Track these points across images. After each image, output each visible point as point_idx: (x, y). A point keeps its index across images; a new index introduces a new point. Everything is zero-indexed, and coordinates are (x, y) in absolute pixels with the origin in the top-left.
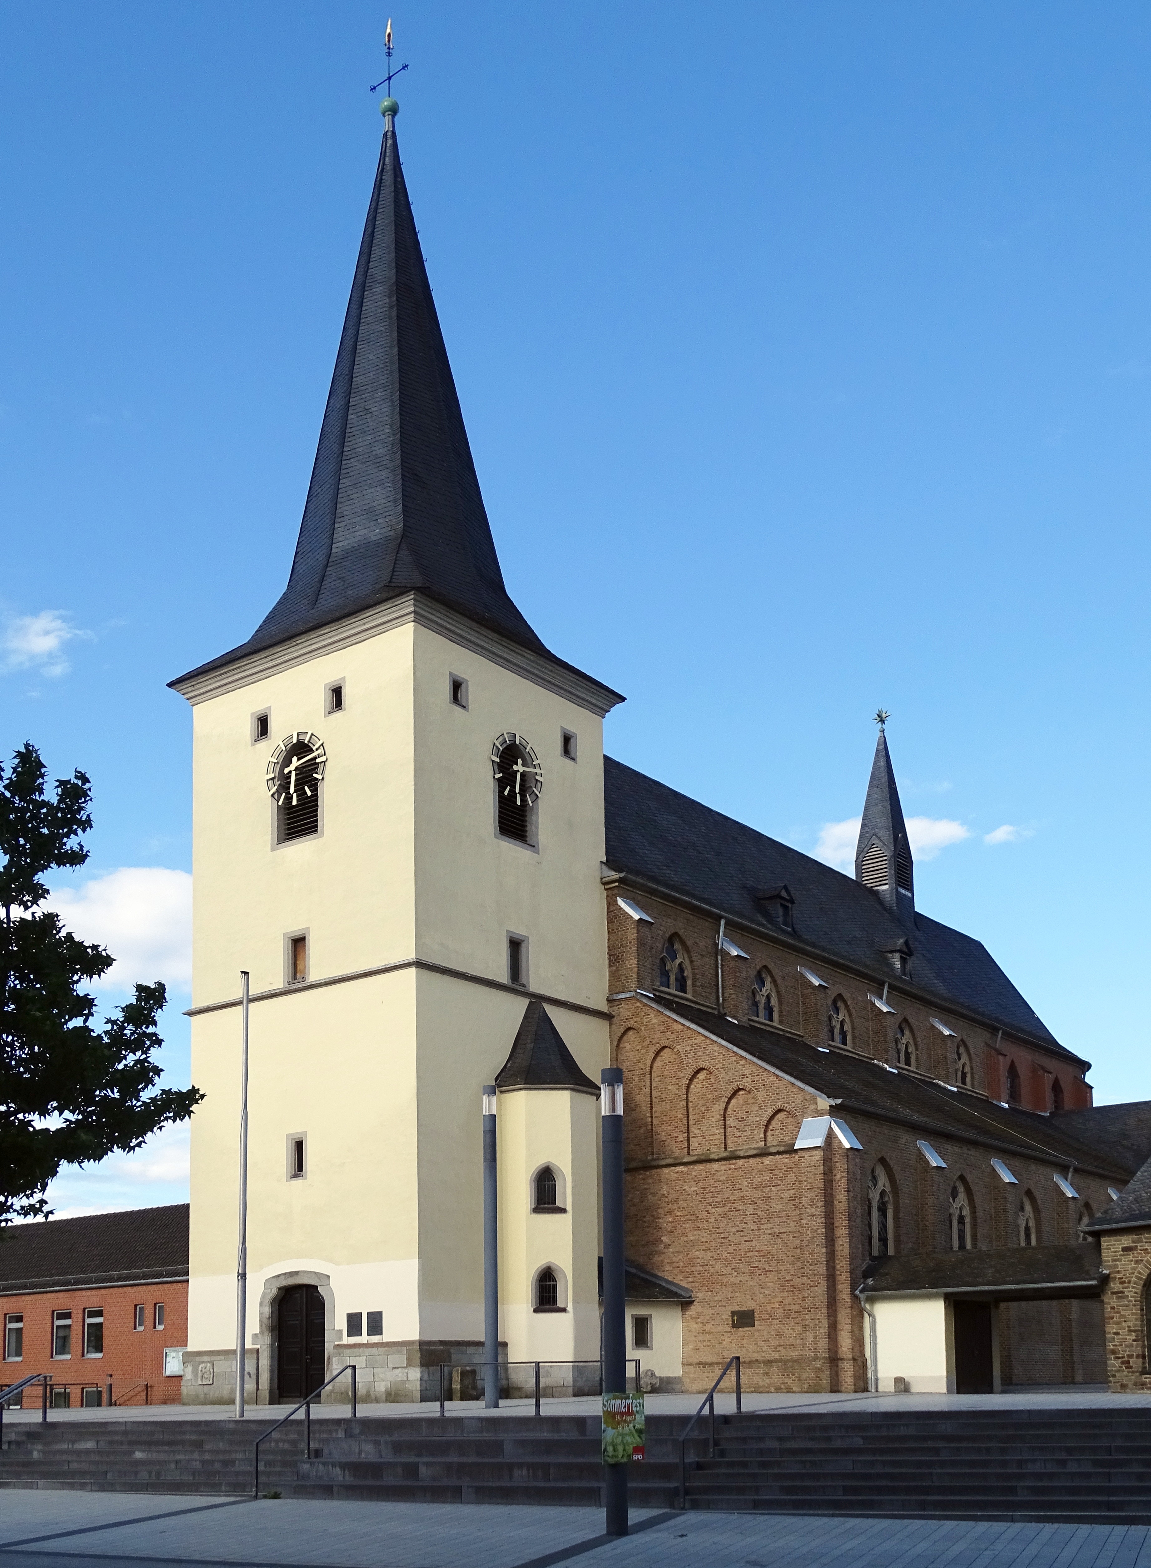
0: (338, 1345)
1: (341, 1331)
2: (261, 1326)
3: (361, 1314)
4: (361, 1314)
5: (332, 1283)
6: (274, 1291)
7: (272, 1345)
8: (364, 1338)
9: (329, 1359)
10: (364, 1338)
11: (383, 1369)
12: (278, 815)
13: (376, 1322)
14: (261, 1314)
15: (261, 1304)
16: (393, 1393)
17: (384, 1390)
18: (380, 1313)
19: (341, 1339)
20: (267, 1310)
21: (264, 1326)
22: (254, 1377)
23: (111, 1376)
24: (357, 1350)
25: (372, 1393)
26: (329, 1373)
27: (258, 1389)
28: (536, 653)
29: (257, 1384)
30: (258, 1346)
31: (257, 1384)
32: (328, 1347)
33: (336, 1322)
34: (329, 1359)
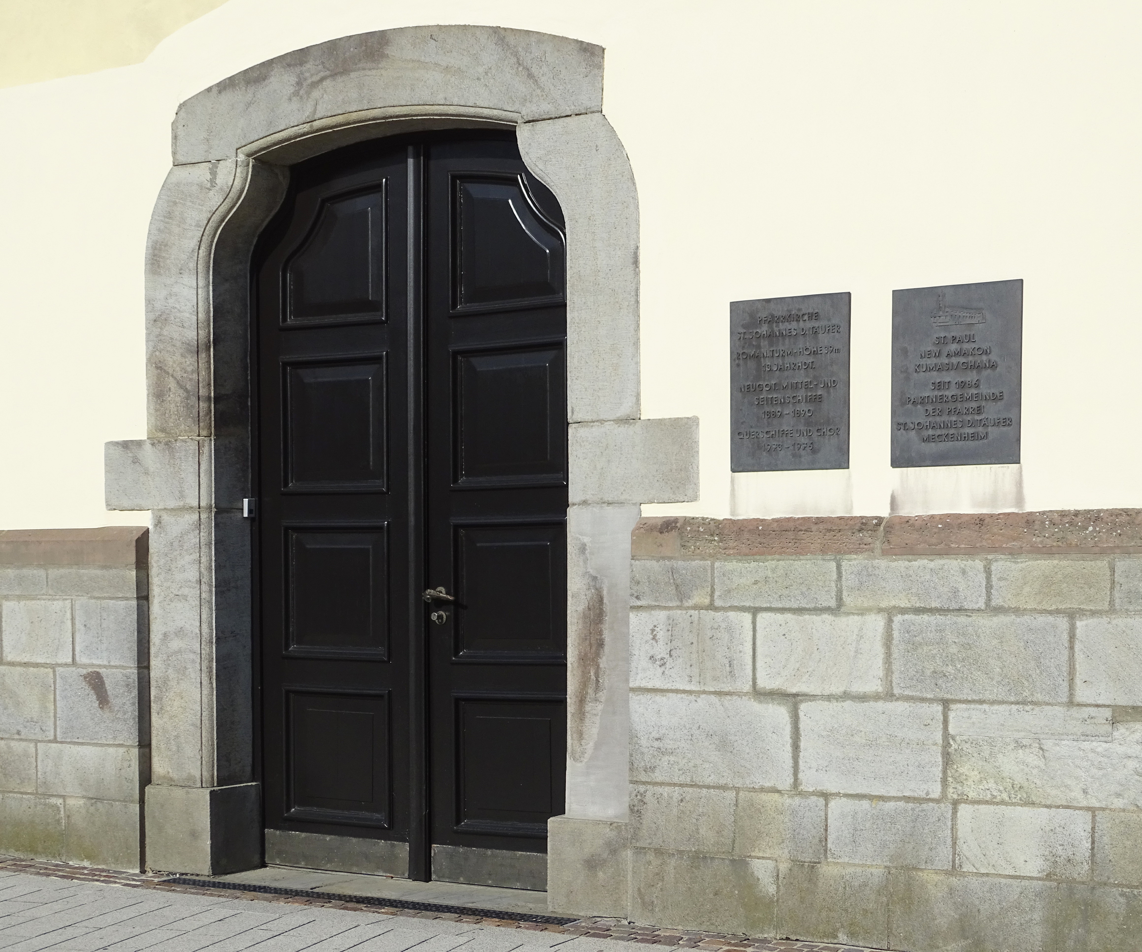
0: (668, 525)
1: (680, 433)
2: (158, 394)
3: (841, 302)
4: (841, 302)
5: (623, 97)
6: (233, 176)
7: (223, 510)
8: (868, 479)
9: (596, 614)
10: (868, 479)
11: (1031, 719)
12: (159, 198)
13: (964, 367)
14: (158, 320)
15: (156, 260)
16: (1114, 901)
17: (1033, 866)
18: (1003, 300)
19: (682, 479)
20: (192, 297)
21: (175, 397)
22: (126, 701)
23: (780, 625)
24: (813, 571)
25: (932, 880)
26: (595, 709)
27: (146, 777)
28: (149, 634)
29: (145, 743)
30: (143, 520)
31: (145, 743)
32: (597, 537)
33: (649, 368)
34: (596, 614)
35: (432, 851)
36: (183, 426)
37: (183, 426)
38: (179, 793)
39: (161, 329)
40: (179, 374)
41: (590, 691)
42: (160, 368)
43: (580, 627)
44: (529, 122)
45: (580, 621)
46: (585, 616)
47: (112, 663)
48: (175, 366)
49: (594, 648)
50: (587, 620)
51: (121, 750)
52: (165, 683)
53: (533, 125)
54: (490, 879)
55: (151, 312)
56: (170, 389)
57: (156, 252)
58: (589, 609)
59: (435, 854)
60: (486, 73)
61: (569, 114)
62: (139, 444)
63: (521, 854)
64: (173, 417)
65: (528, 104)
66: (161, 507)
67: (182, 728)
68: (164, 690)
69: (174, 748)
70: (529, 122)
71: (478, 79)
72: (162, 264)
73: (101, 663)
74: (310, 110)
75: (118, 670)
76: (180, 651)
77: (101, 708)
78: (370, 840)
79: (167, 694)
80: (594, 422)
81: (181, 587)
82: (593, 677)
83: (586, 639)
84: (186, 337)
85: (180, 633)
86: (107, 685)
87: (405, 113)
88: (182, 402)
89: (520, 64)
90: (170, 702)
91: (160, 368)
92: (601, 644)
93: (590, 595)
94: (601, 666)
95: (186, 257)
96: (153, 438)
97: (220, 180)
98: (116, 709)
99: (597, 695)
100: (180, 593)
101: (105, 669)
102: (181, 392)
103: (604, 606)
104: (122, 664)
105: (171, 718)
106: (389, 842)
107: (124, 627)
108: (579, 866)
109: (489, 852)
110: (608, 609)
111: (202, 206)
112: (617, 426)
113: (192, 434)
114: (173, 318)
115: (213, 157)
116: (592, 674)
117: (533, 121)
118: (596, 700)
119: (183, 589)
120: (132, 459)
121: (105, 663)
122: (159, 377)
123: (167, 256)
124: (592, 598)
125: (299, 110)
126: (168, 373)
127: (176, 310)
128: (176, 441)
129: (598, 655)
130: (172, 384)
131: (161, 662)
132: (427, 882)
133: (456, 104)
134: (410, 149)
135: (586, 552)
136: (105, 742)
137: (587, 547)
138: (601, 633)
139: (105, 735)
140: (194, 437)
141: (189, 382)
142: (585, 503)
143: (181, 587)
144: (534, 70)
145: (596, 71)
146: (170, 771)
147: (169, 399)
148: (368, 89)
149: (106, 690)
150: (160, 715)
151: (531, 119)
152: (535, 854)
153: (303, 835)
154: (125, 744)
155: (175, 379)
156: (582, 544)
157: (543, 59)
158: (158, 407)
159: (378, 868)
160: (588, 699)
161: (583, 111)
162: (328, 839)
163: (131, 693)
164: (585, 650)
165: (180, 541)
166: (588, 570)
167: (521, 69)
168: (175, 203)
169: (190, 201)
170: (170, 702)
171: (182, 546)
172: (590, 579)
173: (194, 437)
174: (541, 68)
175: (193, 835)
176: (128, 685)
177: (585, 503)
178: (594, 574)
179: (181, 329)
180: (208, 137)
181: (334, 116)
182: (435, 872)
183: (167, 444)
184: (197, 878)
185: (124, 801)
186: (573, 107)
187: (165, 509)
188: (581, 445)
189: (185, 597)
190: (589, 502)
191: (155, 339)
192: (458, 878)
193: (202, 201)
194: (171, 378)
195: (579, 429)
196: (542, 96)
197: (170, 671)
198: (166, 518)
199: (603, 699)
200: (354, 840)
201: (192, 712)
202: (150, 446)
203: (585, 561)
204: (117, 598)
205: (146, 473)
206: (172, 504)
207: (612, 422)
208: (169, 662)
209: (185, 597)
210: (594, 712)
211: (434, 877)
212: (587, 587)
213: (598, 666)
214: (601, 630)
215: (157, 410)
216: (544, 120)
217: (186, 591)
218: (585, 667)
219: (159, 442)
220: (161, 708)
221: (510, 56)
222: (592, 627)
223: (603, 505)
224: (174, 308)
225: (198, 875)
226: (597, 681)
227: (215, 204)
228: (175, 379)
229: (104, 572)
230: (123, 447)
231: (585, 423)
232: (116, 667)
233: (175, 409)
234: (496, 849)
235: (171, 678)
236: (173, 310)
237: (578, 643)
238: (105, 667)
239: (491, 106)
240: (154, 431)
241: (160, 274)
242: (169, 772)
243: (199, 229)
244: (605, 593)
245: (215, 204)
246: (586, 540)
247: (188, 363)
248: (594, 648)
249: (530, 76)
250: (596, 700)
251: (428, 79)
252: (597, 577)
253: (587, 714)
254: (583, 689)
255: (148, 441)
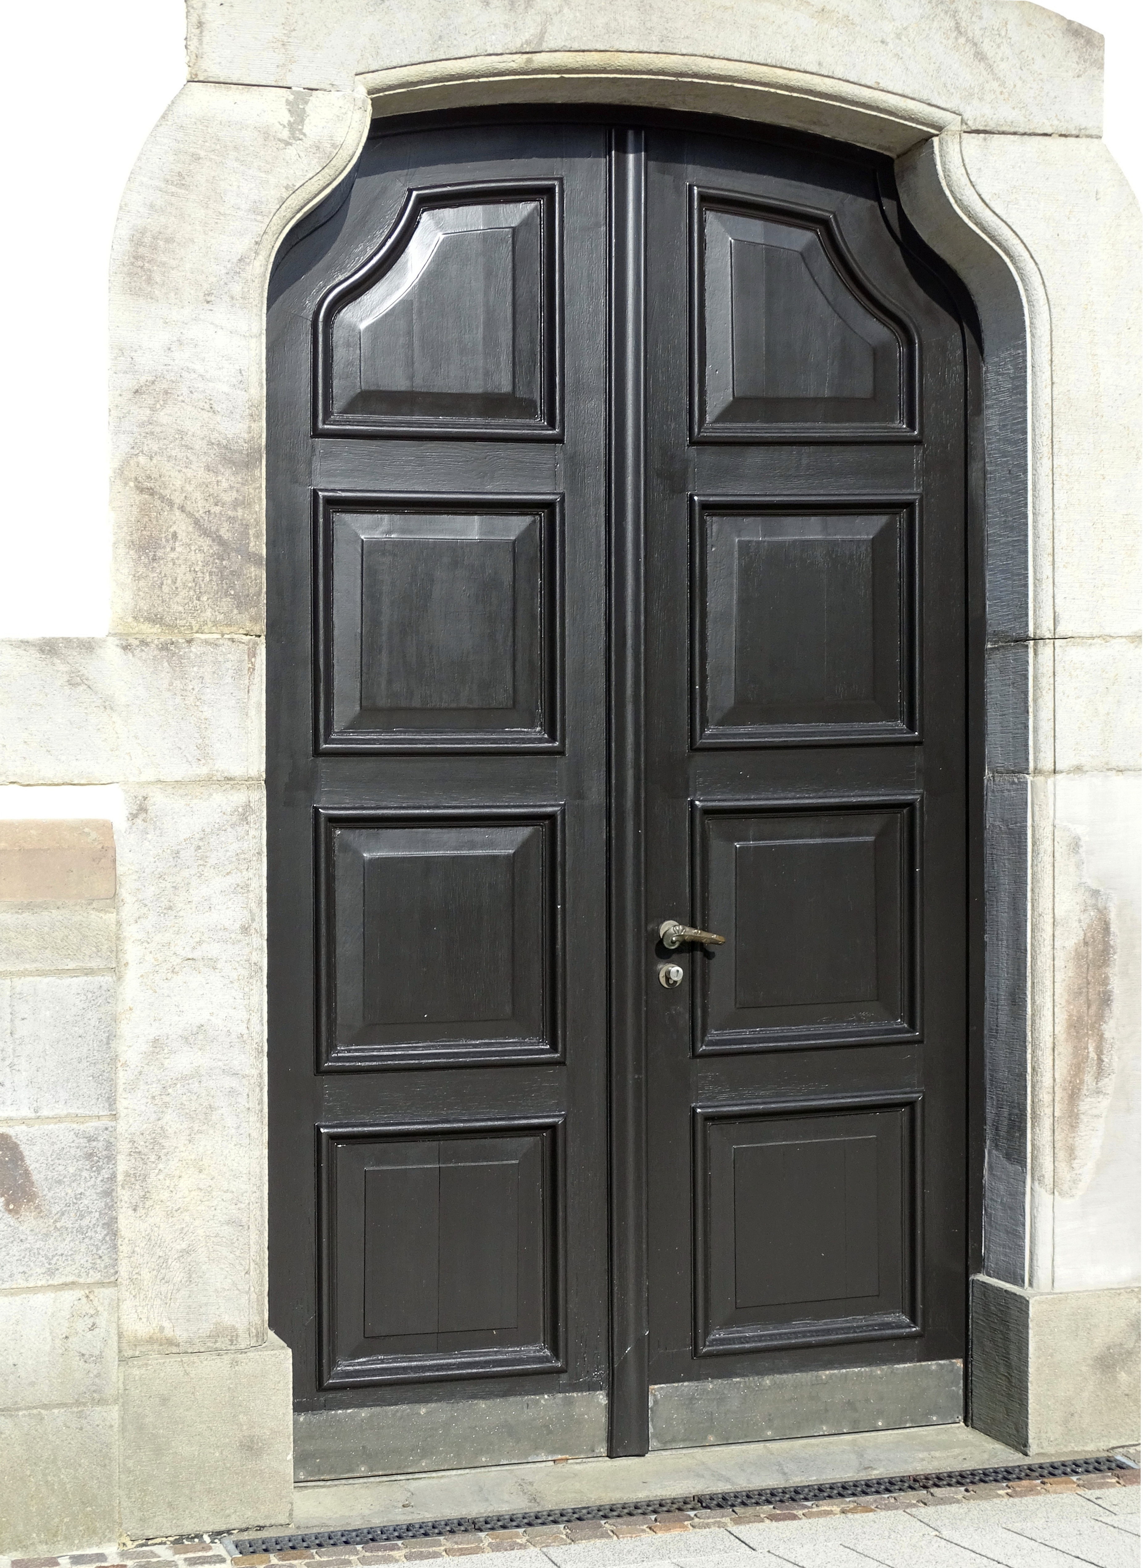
21: (188, 554)
35: (651, 1399)
36: (209, 613)
37: (209, 613)
38: (211, 1368)
39: (153, 409)
40: (199, 506)
41: (1089, 1078)
42: (152, 492)
43: (1071, 974)
44: (978, 132)
45: (1070, 965)
46: (1079, 956)
47: (45, 1112)
48: (189, 488)
49: (1094, 1008)
50: (1083, 962)
51: (69, 1297)
52: (155, 1142)
53: (985, 139)
54: (770, 1428)
55: (125, 372)
56: (175, 535)
57: (141, 250)
58: (1086, 944)
59: (656, 1402)
60: (898, 36)
61: (1049, 131)
62: (88, 646)
63: (831, 1376)
64: (183, 593)
65: (975, 102)
66: (149, 775)
67: (200, 1232)
68: (153, 1158)
69: (179, 1276)
70: (978, 132)
71: (883, 42)
72: (157, 278)
73: (13, 1114)
74: (532, 31)
75: (63, 1126)
76: (196, 1074)
77: (10, 1211)
78: (519, 1398)
79: (161, 1166)
80: (1093, 638)
81: (200, 943)
82: (1093, 1055)
83: (1081, 993)
84: (220, 433)
85: (196, 1036)
86: (28, 1162)
87: (730, 73)
88: (206, 564)
89: (960, 33)
90: (168, 1182)
91: (152, 492)
92: (1106, 1000)
93: (1088, 921)
94: (1107, 1035)
95: (224, 271)
96: (128, 635)
97: (313, 127)
98: (55, 1209)
99: (1100, 1084)
100: (196, 954)
101: (24, 1127)
102: (205, 543)
103: (1112, 937)
104: (72, 1111)
105: (169, 1214)
106: (561, 1395)
107: (81, 1032)
108: (1084, 1369)
109: (767, 1381)
110: (1118, 941)
111: (267, 172)
112: (1132, 645)
113: (233, 629)
114: (185, 391)
115: (298, 78)
116: (1091, 1049)
117: (985, 132)
118: (1098, 1093)
119: (204, 945)
120: (66, 677)
121: (26, 1112)
122: (144, 510)
123: (174, 263)
124: (1090, 926)
125: (506, 26)
126: (171, 504)
127: (194, 376)
128: (189, 642)
129: (1100, 1017)
130: (182, 526)
131: (144, 1100)
132: (641, 1455)
133: (840, 76)
134: (631, 135)
135: (1081, 850)
136: (24, 1284)
137: (1081, 843)
138: (1105, 982)
139: (21, 1269)
140: (236, 636)
141: (225, 525)
142: (1078, 769)
143: (200, 943)
144: (987, 47)
145: (1094, 71)
146: (167, 1324)
147: (173, 555)
148: (661, 17)
149: (27, 1173)
150: (141, 1211)
151: (981, 128)
152: (856, 1370)
153: (364, 1413)
154: (81, 1281)
155: (190, 515)
156: (1074, 838)
157: (1003, 34)
158: (141, 570)
159: (536, 1448)
160: (1084, 1092)
161: (1074, 132)
162: (423, 1411)
163: (98, 1171)
164: (1078, 1011)
165: (199, 847)
166: (1083, 880)
167: (962, 40)
168: (196, 158)
169: (237, 160)
170: (168, 1182)
171: (204, 858)
172: (1087, 894)
173: (236, 636)
174: (999, 46)
175: (250, 1448)
176: (89, 1156)
177: (1078, 769)
178: (1094, 886)
179: (205, 415)
180: (285, 39)
181: (583, 51)
182: (653, 1436)
183: (164, 647)
184: (264, 1534)
185: (78, 1403)
186: (1056, 122)
187: (159, 781)
188: (1070, 675)
189: (212, 963)
190: (1085, 769)
191: (135, 430)
192: (706, 1438)
193: (267, 162)
194: (177, 513)
195: (1067, 649)
196: (1001, 93)
197: (169, 1117)
198: (158, 799)
199: (1110, 1090)
200: (482, 1404)
201: (229, 1196)
202: (119, 650)
203: (1079, 865)
204: (60, 972)
205: (108, 705)
206: (179, 771)
207: (1124, 640)
208: (167, 1099)
209: (212, 963)
210: (1095, 1112)
211: (653, 1443)
212: (1083, 908)
213: (1101, 1037)
214: (1107, 978)
215: (137, 578)
216: (1004, 133)
217: (213, 949)
218: (1079, 1039)
219: (144, 643)
220: (144, 1197)
221: (942, 15)
222: (1091, 973)
223: (1109, 773)
224: (188, 370)
225: (260, 1528)
226: (1100, 1060)
227: (299, 173)
228: (190, 515)
229: (26, 917)
230: (42, 651)
231: (1078, 640)
232: (58, 1119)
233: (189, 577)
234: (781, 1373)
235: (170, 1131)
236: (184, 374)
237: (1067, 1001)
238: (23, 1121)
239: (908, 92)
240: (130, 620)
241: (151, 297)
242: (162, 1329)
243: (259, 218)
244: (1113, 916)
245: (299, 173)
246: (1080, 830)
247: (225, 485)
248: (1094, 1008)
249: (980, 56)
250: (1098, 1092)
251: (786, 23)
252: (1099, 891)
253: (1082, 1116)
254: (1076, 1075)
255: (112, 642)
